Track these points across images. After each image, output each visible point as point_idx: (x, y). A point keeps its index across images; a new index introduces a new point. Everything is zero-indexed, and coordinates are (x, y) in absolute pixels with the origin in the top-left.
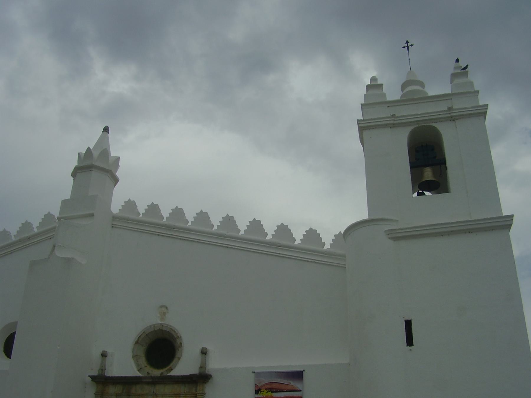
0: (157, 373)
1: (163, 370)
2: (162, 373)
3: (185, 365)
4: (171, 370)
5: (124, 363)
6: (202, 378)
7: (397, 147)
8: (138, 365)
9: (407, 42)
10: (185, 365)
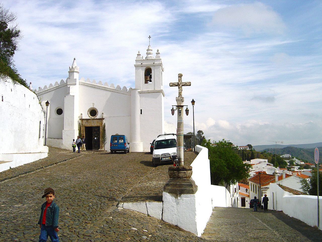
0: (93, 117)
2: (94, 118)
3: (98, 116)
5: (86, 116)
6: (102, 119)
7: (142, 73)
8: (89, 116)
9: (150, 36)
10: (98, 116)
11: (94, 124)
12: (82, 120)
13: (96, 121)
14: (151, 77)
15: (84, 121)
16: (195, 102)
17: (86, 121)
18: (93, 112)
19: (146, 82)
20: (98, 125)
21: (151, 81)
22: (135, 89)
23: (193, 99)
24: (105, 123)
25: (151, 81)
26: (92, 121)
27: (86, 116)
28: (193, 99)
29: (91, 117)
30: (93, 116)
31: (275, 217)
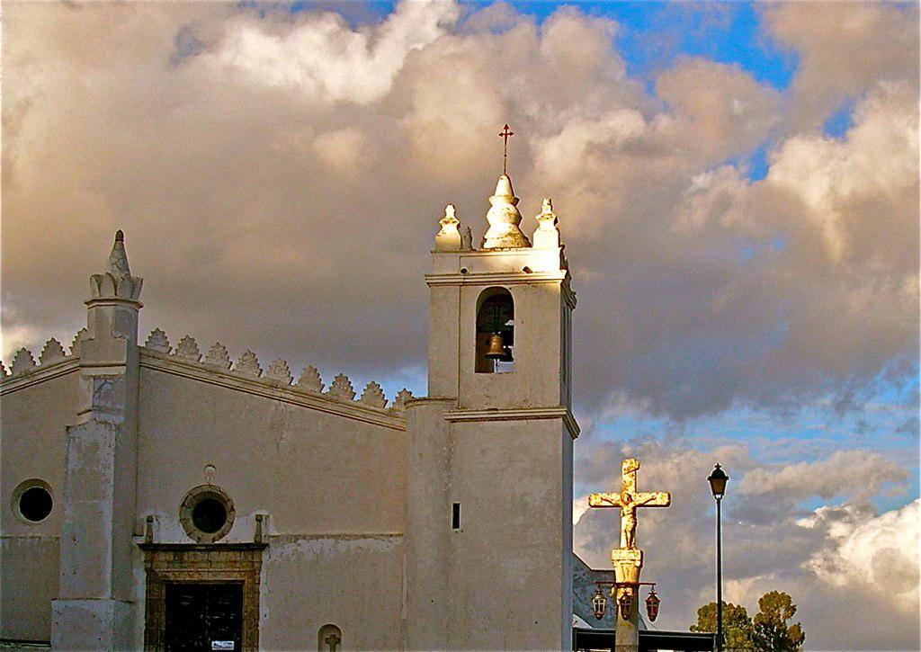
0: (208, 538)
1: (215, 535)
3: (241, 531)
4: (223, 535)
5: (172, 531)
6: (258, 547)
9: (506, 128)
10: (241, 531)
11: (215, 571)
12: (151, 548)
13: (223, 556)
14: (508, 337)
15: (162, 556)
16: (727, 478)
17: (170, 556)
18: (209, 511)
19: (484, 365)
20: (235, 577)
21: (507, 357)
22: (425, 399)
23: (718, 467)
24: (804, 634)
25: (507, 357)
26: (206, 556)
27: (172, 531)
28: (718, 467)
29: (199, 533)
30: (210, 532)
31: (560, 291)
